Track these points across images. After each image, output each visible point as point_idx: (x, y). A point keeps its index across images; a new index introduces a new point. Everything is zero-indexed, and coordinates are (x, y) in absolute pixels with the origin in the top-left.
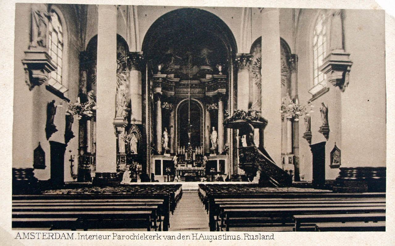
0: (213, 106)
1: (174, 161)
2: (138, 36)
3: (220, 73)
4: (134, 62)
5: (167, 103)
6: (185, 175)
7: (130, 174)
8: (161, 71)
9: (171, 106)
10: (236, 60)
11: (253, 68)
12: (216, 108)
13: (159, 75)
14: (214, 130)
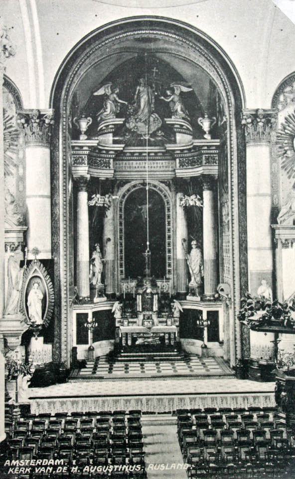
0: (192, 200)
5: (98, 196)
6: (137, 343)
7: (28, 381)
8: (86, 133)
9: (106, 199)
11: (278, 137)
12: (198, 204)
13: (83, 140)
14: (194, 246)
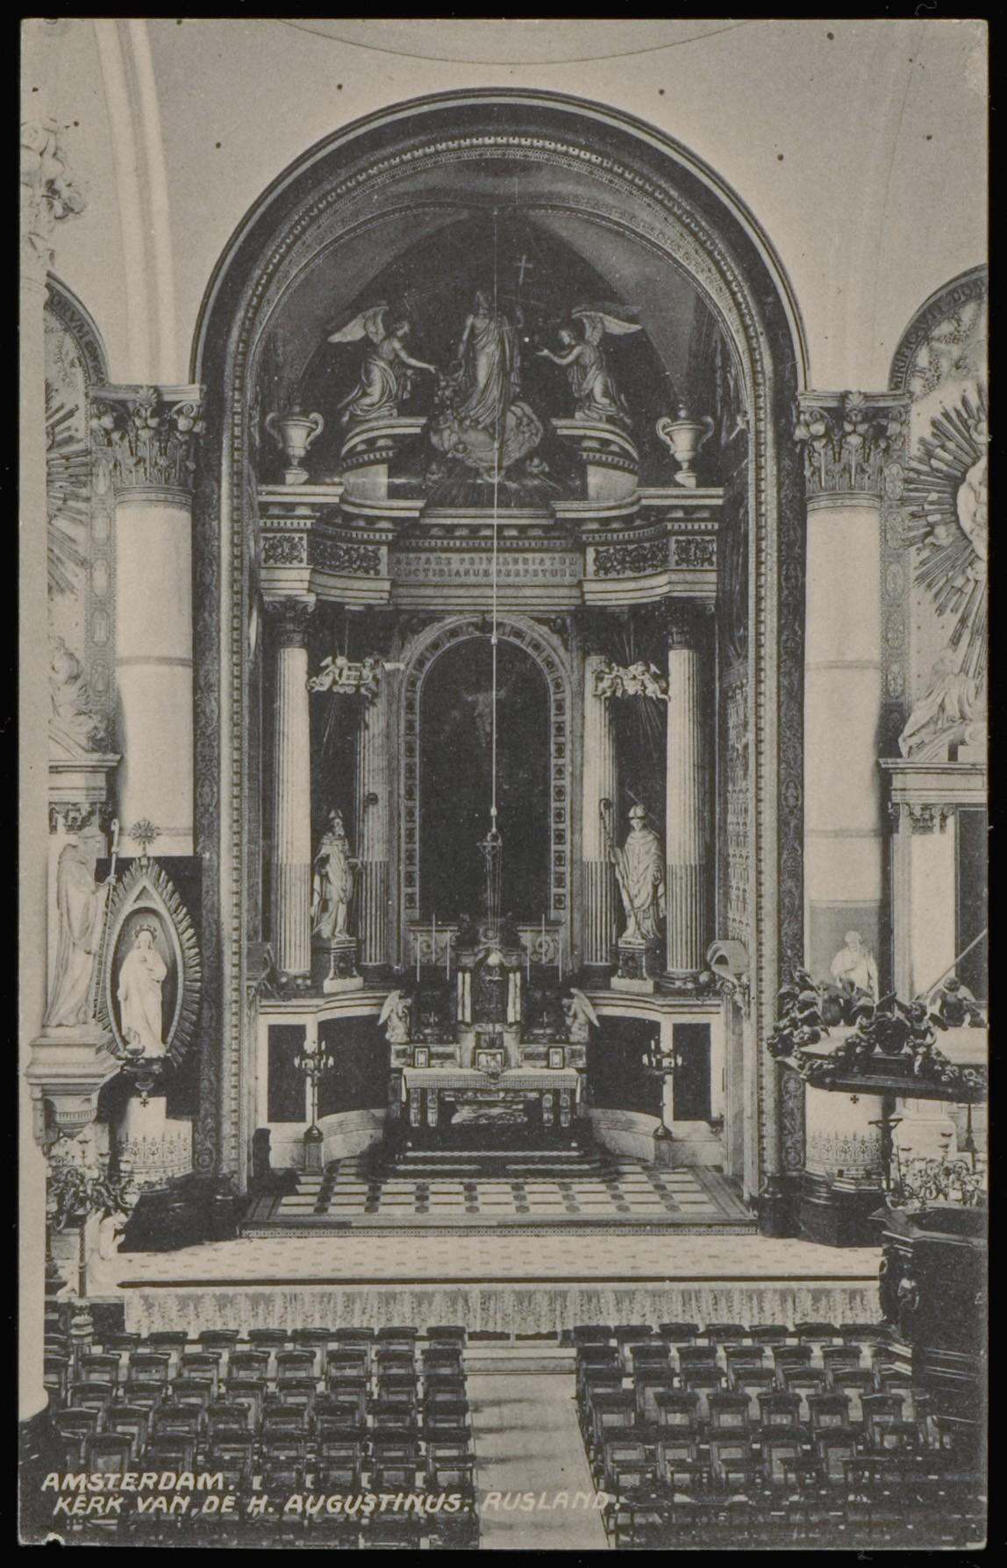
1: (385, 1027)
2: (164, 262)
3: (685, 478)
4: (143, 452)
6: (456, 1119)
8: (304, 463)
9: (366, 672)
10: (800, 433)
11: (906, 481)
12: (652, 689)
13: (295, 486)
